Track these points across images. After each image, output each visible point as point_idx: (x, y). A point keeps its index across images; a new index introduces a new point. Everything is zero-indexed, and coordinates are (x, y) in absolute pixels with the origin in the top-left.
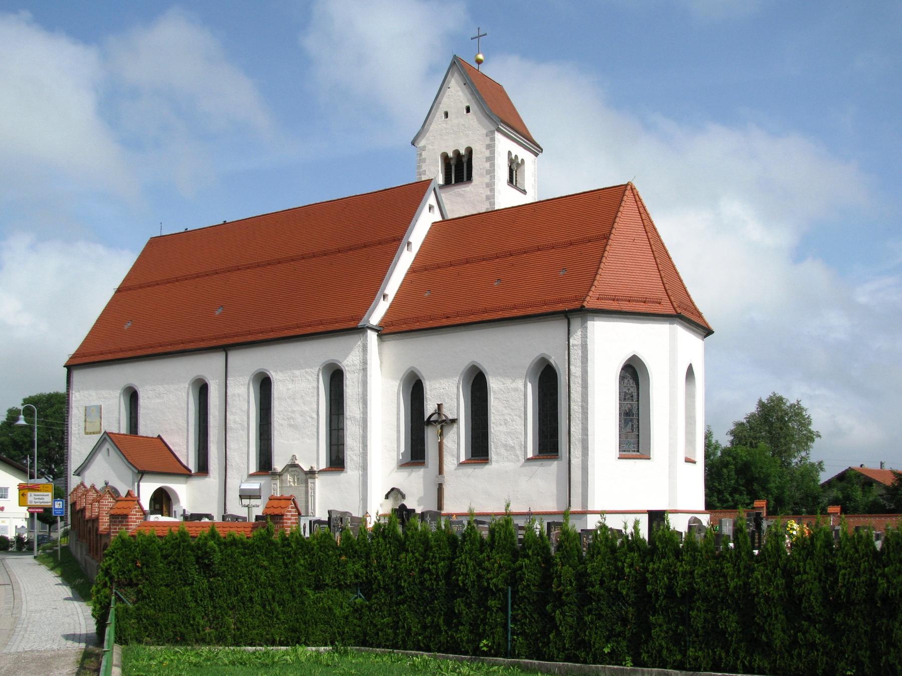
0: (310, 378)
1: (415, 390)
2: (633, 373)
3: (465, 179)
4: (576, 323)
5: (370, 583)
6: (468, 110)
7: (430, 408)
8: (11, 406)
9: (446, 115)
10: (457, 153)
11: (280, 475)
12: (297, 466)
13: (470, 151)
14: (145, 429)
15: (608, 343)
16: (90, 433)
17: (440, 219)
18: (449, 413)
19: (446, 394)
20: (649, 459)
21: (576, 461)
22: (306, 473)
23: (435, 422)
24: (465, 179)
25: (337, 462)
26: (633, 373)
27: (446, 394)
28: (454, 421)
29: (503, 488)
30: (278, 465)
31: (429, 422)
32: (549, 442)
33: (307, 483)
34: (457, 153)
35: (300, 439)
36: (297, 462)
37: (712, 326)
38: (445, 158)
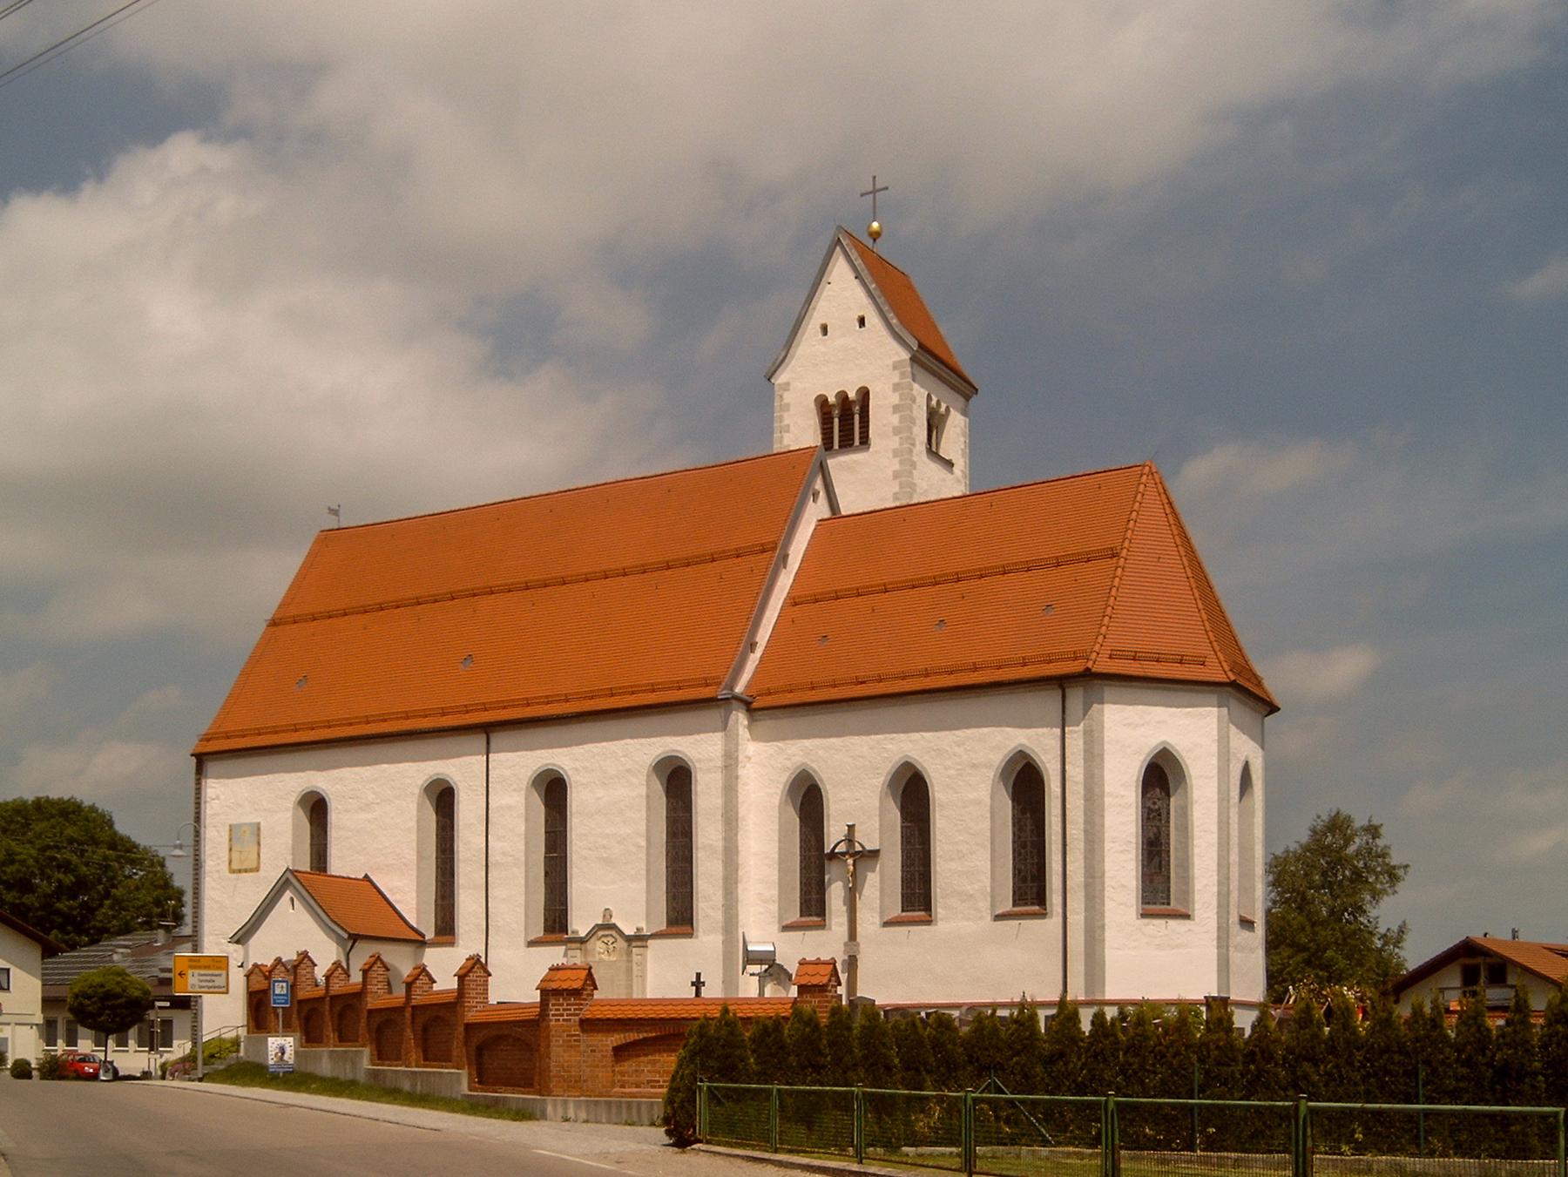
0: (634, 780)
1: (808, 799)
2: (1161, 776)
3: (857, 443)
4: (1076, 697)
5: (1308, 962)
6: (862, 322)
7: (834, 834)
8: (1346, 810)
9: (825, 330)
10: (843, 397)
11: (582, 941)
12: (613, 927)
13: (864, 394)
14: (340, 863)
15: (1131, 729)
16: (240, 871)
17: (827, 514)
18: (868, 839)
19: (859, 809)
20: (1187, 917)
21: (1077, 919)
22: (629, 939)
23: (843, 854)
24: (857, 443)
25: (681, 918)
26: (1161, 776)
27: (859, 809)
28: (875, 854)
29: (957, 960)
30: (580, 924)
31: (833, 855)
32: (1030, 887)
33: (629, 953)
34: (843, 397)
35: (614, 879)
36: (613, 921)
37: (1277, 700)
38: (822, 404)
